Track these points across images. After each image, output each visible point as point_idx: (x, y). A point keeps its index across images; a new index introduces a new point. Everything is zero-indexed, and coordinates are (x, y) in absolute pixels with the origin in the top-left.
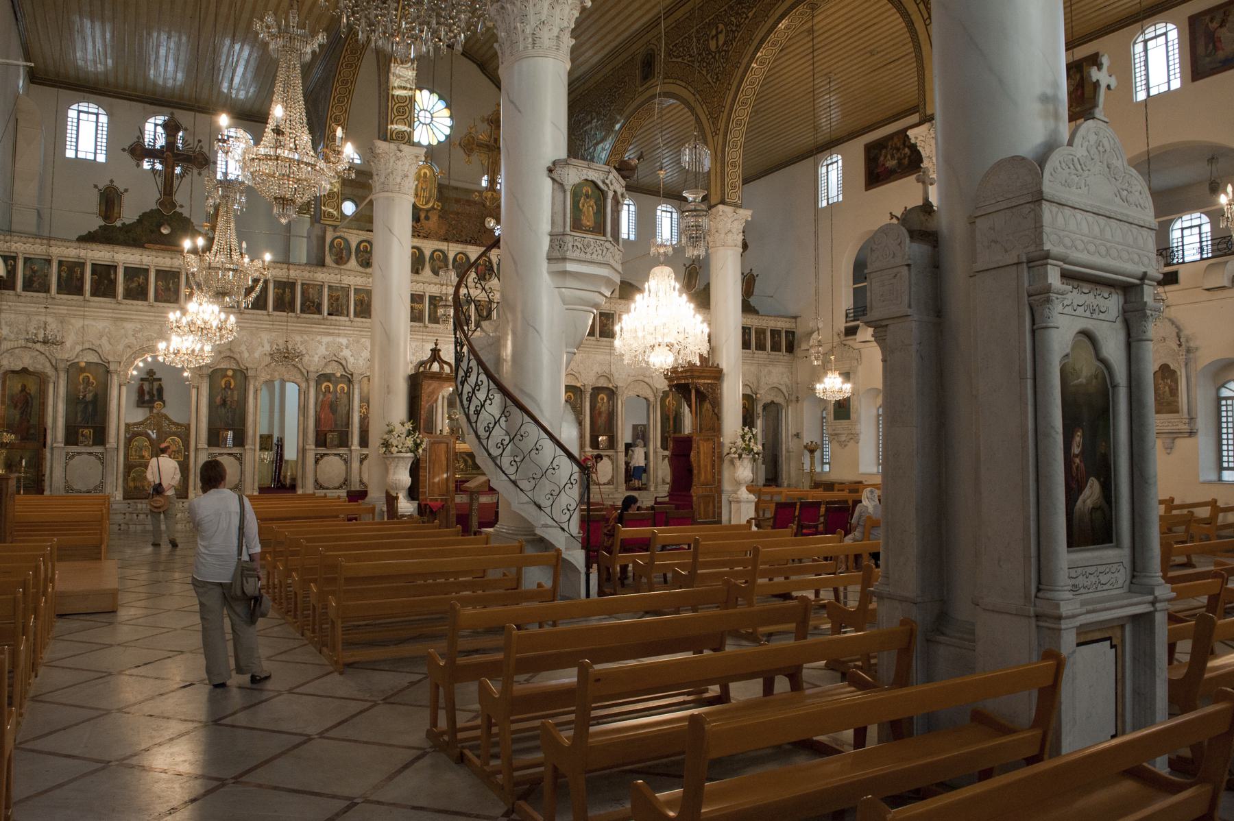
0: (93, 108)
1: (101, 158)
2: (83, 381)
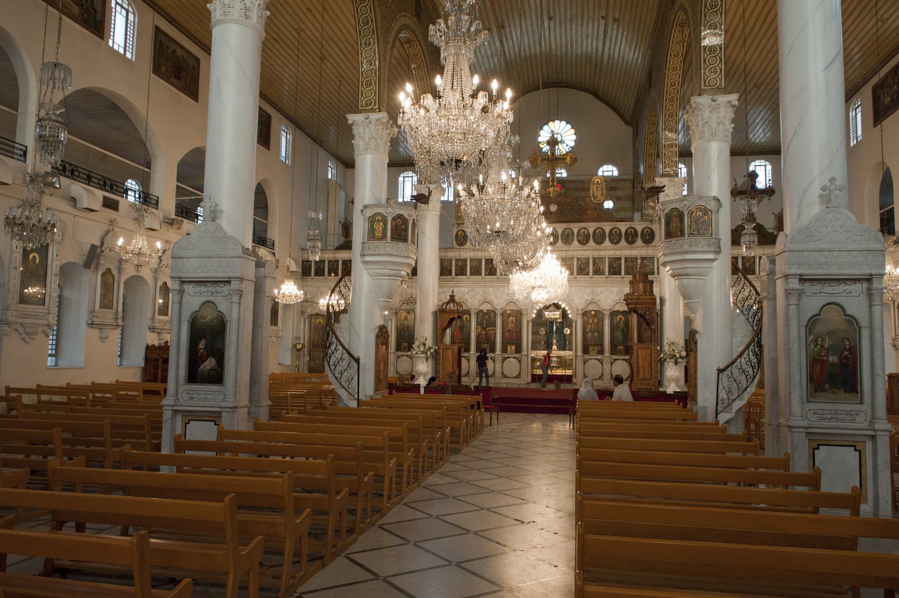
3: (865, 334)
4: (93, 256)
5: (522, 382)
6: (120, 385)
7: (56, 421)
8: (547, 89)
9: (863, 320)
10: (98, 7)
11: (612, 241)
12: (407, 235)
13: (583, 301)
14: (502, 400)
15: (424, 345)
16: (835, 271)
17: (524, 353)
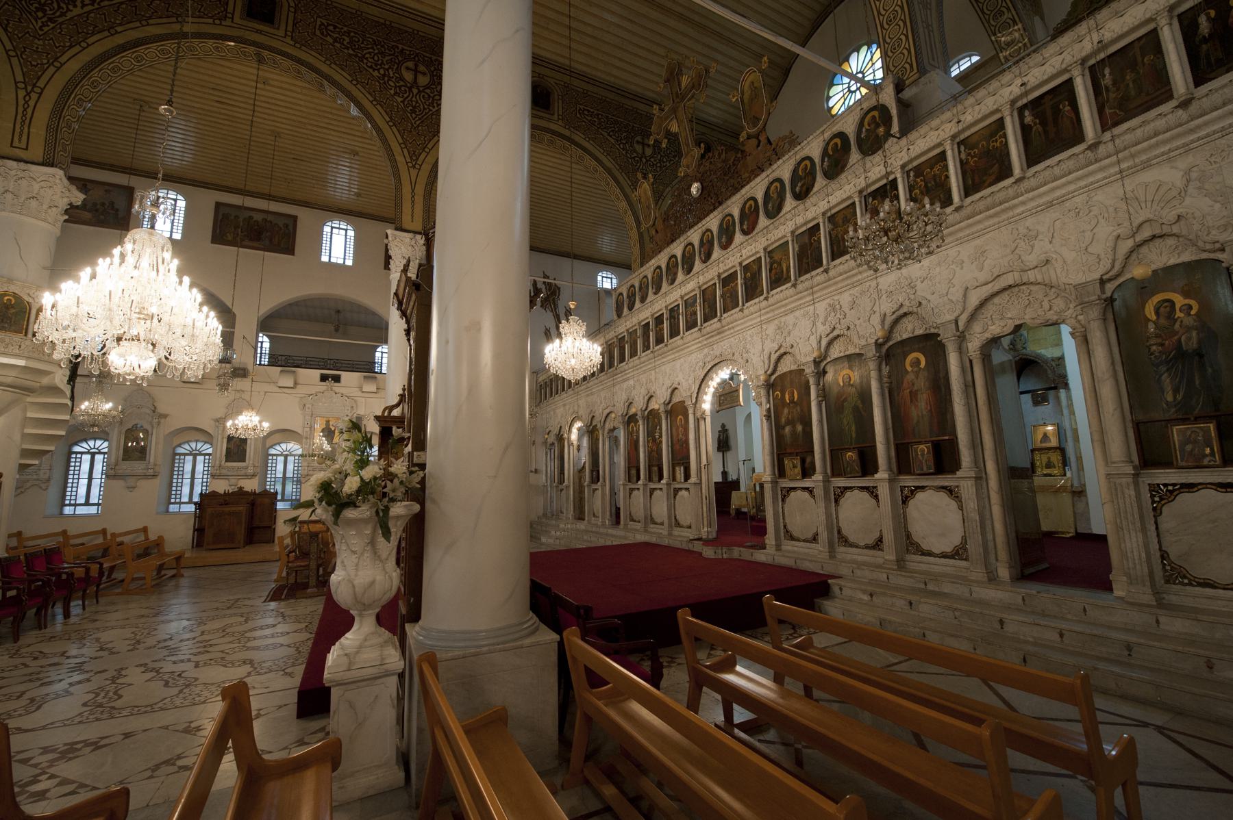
0: (343, 225)
1: (349, 262)
2: (1157, 313)
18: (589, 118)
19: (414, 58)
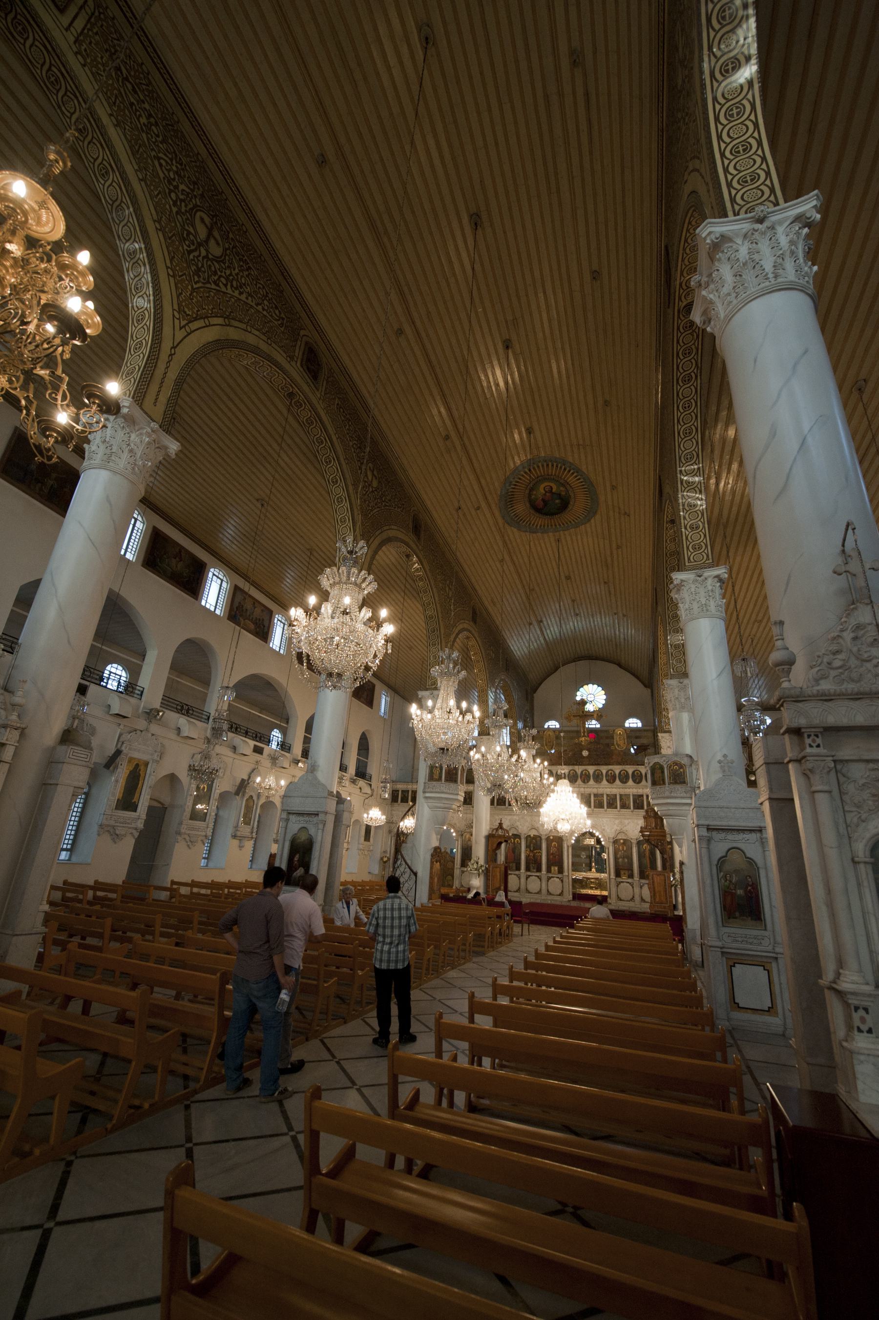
3: (762, 873)
4: (243, 786)
5: (564, 900)
6: (248, 884)
7: (516, 1240)
8: (574, 663)
9: (760, 863)
10: (266, 624)
11: (634, 781)
12: (457, 778)
13: (613, 830)
14: (532, 913)
15: (477, 863)
16: (733, 823)
17: (566, 873)
18: (343, 418)
19: (213, 216)
